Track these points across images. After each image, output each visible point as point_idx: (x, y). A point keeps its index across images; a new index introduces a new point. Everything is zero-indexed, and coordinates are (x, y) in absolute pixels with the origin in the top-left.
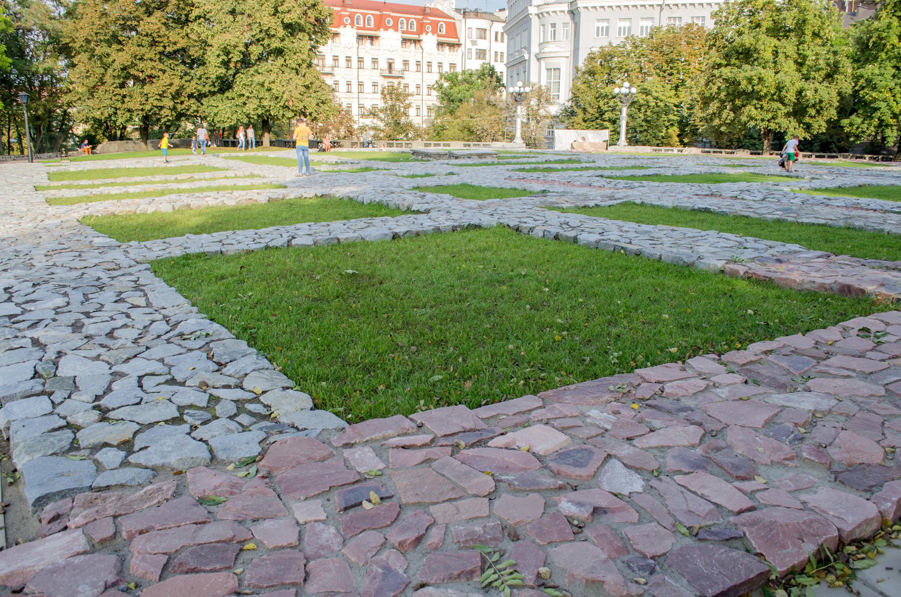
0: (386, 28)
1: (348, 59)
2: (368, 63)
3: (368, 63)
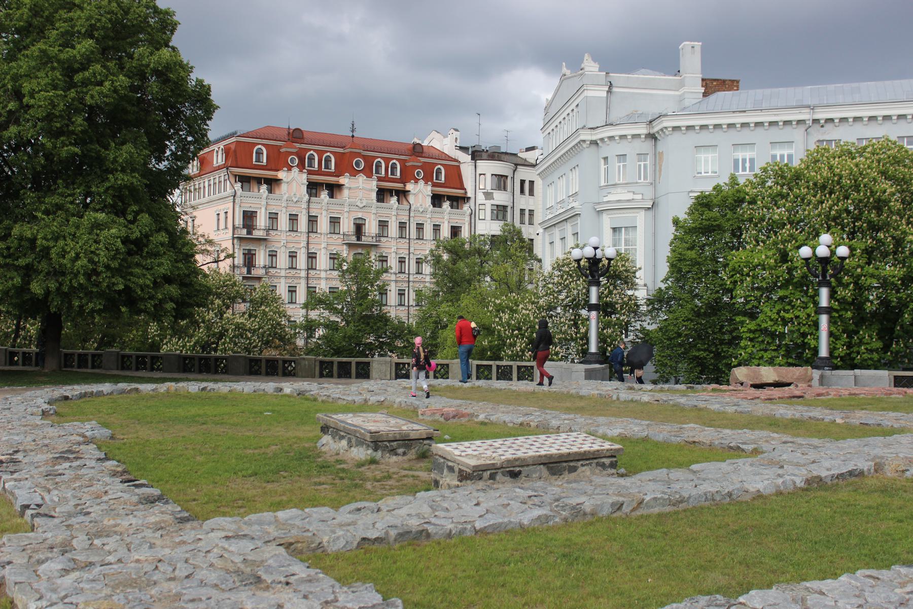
0: (354, 173)
1: (293, 218)
2: (323, 225)
3: (323, 225)
